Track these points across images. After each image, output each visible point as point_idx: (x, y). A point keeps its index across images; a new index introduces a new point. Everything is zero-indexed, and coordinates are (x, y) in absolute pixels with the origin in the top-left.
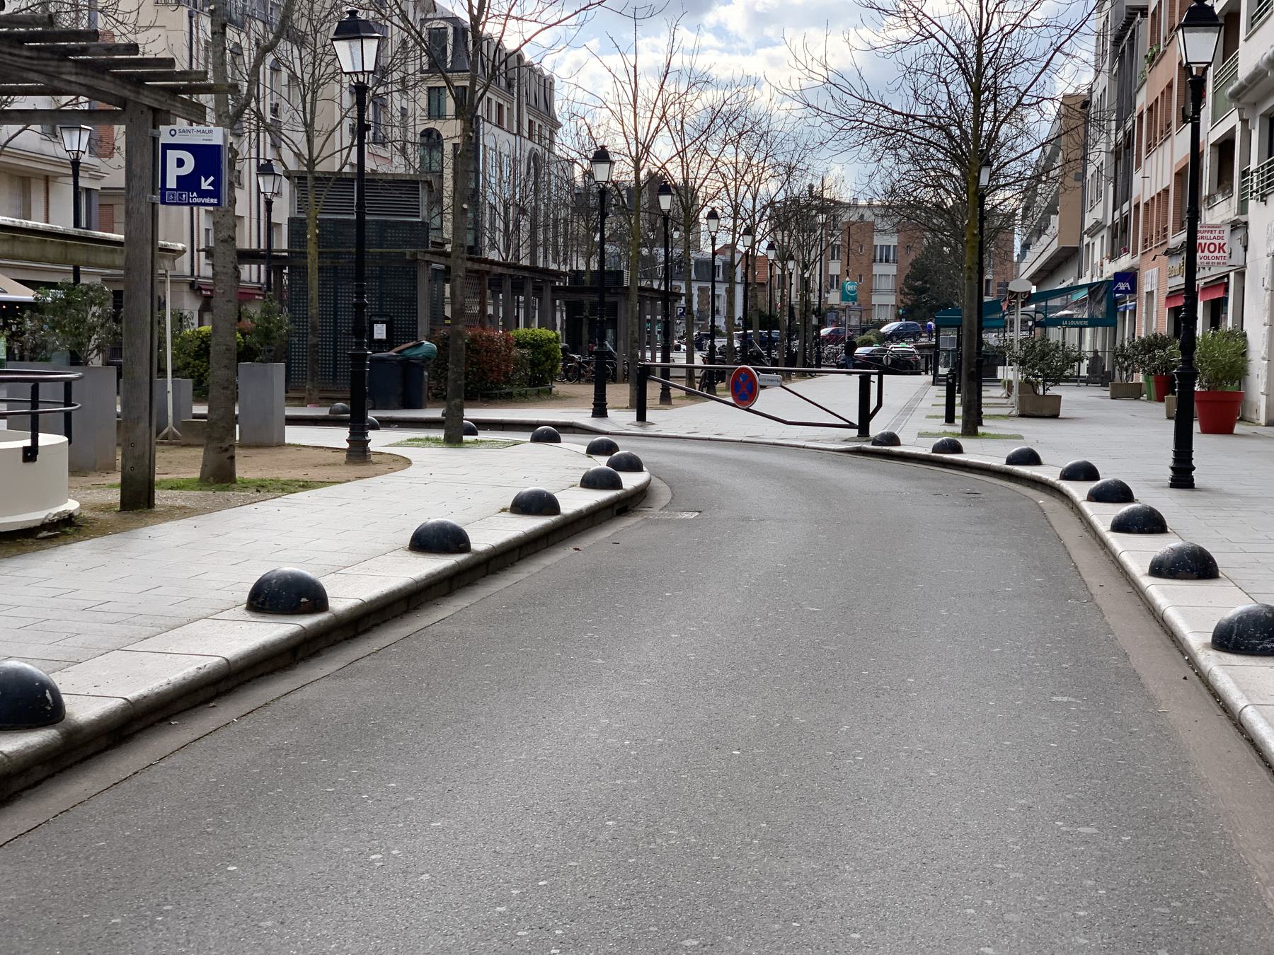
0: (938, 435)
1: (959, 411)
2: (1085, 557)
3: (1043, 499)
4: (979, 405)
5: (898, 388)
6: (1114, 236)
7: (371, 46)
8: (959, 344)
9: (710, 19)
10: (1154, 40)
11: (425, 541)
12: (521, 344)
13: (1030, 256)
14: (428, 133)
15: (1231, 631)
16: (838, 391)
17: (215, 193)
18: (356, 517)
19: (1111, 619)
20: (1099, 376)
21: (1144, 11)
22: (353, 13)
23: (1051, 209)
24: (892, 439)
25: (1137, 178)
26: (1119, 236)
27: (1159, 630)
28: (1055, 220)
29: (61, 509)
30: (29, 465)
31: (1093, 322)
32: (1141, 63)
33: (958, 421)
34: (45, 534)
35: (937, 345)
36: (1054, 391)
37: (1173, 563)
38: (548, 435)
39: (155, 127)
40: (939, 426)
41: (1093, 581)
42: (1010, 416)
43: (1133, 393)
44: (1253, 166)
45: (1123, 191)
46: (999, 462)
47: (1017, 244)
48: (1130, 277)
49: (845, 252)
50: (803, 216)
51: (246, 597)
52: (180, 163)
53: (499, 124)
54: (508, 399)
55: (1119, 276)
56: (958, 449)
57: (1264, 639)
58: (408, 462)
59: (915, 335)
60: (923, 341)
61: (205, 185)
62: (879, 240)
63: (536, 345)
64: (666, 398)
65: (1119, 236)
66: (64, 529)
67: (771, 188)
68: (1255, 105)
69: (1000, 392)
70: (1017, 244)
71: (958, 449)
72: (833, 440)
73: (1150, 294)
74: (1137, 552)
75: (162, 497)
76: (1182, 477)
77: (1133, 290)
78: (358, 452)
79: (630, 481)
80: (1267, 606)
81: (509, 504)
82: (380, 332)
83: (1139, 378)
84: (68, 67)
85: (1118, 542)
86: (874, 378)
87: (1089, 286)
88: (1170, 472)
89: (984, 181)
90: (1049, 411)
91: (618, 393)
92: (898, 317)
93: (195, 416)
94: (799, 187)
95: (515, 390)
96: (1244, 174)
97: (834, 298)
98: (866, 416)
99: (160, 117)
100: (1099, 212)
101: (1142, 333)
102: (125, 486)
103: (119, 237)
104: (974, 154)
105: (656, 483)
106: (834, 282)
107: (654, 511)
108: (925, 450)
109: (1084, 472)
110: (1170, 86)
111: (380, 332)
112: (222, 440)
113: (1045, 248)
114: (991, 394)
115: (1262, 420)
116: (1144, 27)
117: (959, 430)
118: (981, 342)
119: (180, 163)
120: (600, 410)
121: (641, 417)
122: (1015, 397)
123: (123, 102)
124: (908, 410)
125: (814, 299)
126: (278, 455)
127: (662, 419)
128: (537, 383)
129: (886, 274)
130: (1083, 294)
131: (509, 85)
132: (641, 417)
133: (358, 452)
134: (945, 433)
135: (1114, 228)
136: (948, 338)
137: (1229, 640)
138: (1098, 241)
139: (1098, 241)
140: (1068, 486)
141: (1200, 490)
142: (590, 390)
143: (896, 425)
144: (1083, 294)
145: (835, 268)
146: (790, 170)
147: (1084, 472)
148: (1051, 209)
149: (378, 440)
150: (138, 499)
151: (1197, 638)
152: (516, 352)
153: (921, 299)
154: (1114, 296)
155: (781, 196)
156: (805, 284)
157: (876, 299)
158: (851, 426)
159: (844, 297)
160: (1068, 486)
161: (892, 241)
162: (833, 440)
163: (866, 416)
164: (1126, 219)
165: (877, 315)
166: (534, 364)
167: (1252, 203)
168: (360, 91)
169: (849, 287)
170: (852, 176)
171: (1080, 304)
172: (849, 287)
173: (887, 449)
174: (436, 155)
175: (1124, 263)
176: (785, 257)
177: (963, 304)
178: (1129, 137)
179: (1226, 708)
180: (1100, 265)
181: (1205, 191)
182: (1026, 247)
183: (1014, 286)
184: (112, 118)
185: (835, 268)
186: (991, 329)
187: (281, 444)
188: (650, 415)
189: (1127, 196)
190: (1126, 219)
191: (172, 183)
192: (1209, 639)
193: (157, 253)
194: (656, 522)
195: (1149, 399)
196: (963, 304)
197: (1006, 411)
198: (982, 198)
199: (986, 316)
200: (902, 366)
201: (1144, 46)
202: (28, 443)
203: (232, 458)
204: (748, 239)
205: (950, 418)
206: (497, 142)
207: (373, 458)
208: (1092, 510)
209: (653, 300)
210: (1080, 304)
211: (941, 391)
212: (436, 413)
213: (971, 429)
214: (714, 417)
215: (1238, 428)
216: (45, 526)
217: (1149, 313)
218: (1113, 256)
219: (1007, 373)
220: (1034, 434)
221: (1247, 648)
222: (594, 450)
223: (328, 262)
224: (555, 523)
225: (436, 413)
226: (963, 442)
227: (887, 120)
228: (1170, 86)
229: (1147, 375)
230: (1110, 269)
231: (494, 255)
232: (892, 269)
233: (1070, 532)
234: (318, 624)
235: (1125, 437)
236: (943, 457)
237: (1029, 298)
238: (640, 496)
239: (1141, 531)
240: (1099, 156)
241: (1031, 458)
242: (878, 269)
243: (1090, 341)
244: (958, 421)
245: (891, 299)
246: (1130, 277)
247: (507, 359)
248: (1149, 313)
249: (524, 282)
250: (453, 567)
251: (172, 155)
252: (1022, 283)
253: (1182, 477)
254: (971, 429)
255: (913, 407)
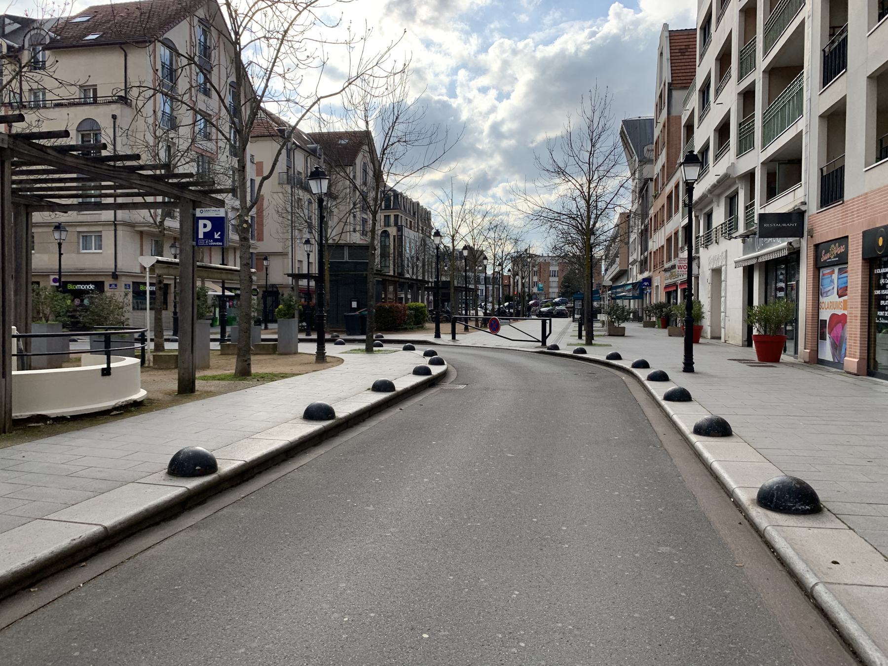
0: (575, 345)
1: (584, 333)
2: (651, 413)
3: (624, 377)
4: (592, 331)
5: (558, 324)
6: (641, 265)
7: (325, 183)
8: (583, 306)
9: (490, 192)
10: (656, 190)
11: (311, 414)
12: (410, 309)
13: (609, 273)
14: (385, 232)
15: (773, 495)
16: (533, 326)
17: (221, 240)
18: (349, 376)
19: (676, 461)
20: (638, 319)
21: (651, 179)
22: (316, 168)
23: (616, 256)
24: (556, 347)
25: (650, 243)
26: (643, 265)
27: (708, 474)
28: (618, 260)
29: (128, 399)
30: (107, 377)
31: (634, 298)
32: (651, 199)
33: (584, 338)
34: (115, 413)
35: (574, 307)
36: (622, 325)
37: (708, 427)
38: (409, 346)
39: (194, 209)
40: (575, 340)
41: (671, 449)
42: (604, 335)
43: (652, 325)
44: (701, 234)
45: (645, 248)
46: (603, 358)
47: (603, 268)
48: (649, 280)
49: (538, 273)
50: (522, 260)
51: (166, 466)
52: (205, 226)
53: (411, 228)
54: (405, 330)
55: (644, 280)
56: (584, 352)
57: (796, 503)
58: (341, 361)
59: (565, 303)
60: (569, 305)
61: (216, 236)
62: (552, 268)
63: (417, 309)
64: (466, 329)
65: (643, 265)
66: (135, 407)
67: (509, 248)
68: (701, 210)
69: (600, 325)
70: (603, 268)
71: (584, 352)
72: (531, 347)
73: (657, 286)
74: (659, 390)
75: (199, 385)
76: (689, 367)
77: (650, 285)
78: (321, 357)
79: (436, 370)
80: (795, 479)
81: (371, 387)
82: (354, 305)
83: (654, 319)
84: (135, 176)
85: (649, 384)
86: (548, 321)
87: (632, 284)
88: (683, 365)
89: (592, 241)
90: (620, 333)
91: (446, 327)
92: (559, 297)
93: (263, 340)
94: (522, 247)
95: (408, 327)
96: (697, 238)
97: (535, 290)
98: (544, 337)
99: (196, 204)
100: (635, 255)
101: (654, 301)
102: (181, 382)
103: (238, 268)
104: (588, 232)
105: (451, 369)
106: (535, 284)
107: (446, 385)
108: (571, 353)
109: (643, 364)
110: (663, 206)
111: (354, 305)
112: (244, 356)
113: (615, 269)
114: (597, 325)
115: (709, 337)
116: (652, 185)
117: (584, 342)
118: (592, 306)
119: (205, 226)
120: (438, 335)
121: (454, 338)
122: (606, 328)
123: (177, 197)
124: (563, 333)
125: (527, 290)
126: (295, 358)
127: (464, 339)
128: (417, 322)
129: (554, 281)
130: (630, 287)
131: (414, 214)
132: (454, 338)
133: (321, 357)
134: (578, 344)
135: (641, 262)
136: (578, 305)
137: (771, 502)
138: (635, 267)
139: (635, 267)
140: (636, 371)
141: (697, 373)
142: (433, 325)
143: (557, 340)
144: (630, 287)
145: (535, 279)
146: (516, 241)
147: (643, 364)
148: (616, 256)
149: (331, 350)
150: (187, 389)
151: (746, 496)
152: (408, 312)
153: (568, 290)
154: (642, 288)
155: (513, 251)
156: (523, 284)
157: (551, 290)
158: (539, 341)
159: (539, 289)
160: (636, 371)
161: (557, 268)
162: (531, 347)
163: (544, 337)
164: (646, 258)
165: (551, 296)
166: (416, 316)
167: (701, 249)
168: (320, 201)
169: (540, 285)
170: (541, 244)
171: (629, 291)
172: (540, 285)
173: (553, 352)
174: (387, 240)
175: (646, 275)
176: (516, 274)
177: (584, 290)
178: (646, 226)
179: (782, 561)
180: (636, 276)
181: (680, 245)
182: (606, 270)
183: (604, 284)
184: (175, 205)
185: (535, 279)
186: (597, 300)
187: (296, 353)
188: (457, 337)
189: (646, 249)
190: (646, 258)
191: (201, 236)
192: (755, 495)
193: (196, 269)
194: (445, 391)
195: (659, 327)
196: (584, 290)
197: (603, 333)
198: (591, 248)
199: (594, 294)
200: (561, 315)
201: (652, 191)
202: (105, 366)
203: (249, 364)
204: (500, 268)
205: (580, 337)
206: (411, 236)
207: (328, 359)
208: (706, 447)
209: (462, 291)
210: (629, 291)
211: (576, 325)
212: (364, 337)
213: (589, 342)
214: (481, 338)
215: (701, 340)
216: (115, 408)
217: (657, 293)
218: (641, 272)
219: (602, 317)
220: (617, 344)
221: (784, 509)
222: (427, 354)
223: (334, 278)
224: (391, 396)
225: (364, 337)
226: (586, 348)
227: (551, 215)
228: (663, 206)
229: (658, 318)
230: (640, 277)
231: (407, 276)
232: (556, 279)
233: (640, 396)
234: (209, 482)
235: (662, 348)
236: (578, 355)
237: (611, 288)
238: (443, 376)
239: (679, 400)
240: (634, 236)
241: (617, 357)
242: (551, 279)
243: (633, 305)
244: (584, 338)
245: (557, 290)
246: (649, 280)
247: (405, 315)
248: (657, 293)
249: (416, 285)
250: (320, 430)
251: (201, 223)
252: (607, 280)
253: (689, 367)
254: (589, 342)
255: (564, 332)
